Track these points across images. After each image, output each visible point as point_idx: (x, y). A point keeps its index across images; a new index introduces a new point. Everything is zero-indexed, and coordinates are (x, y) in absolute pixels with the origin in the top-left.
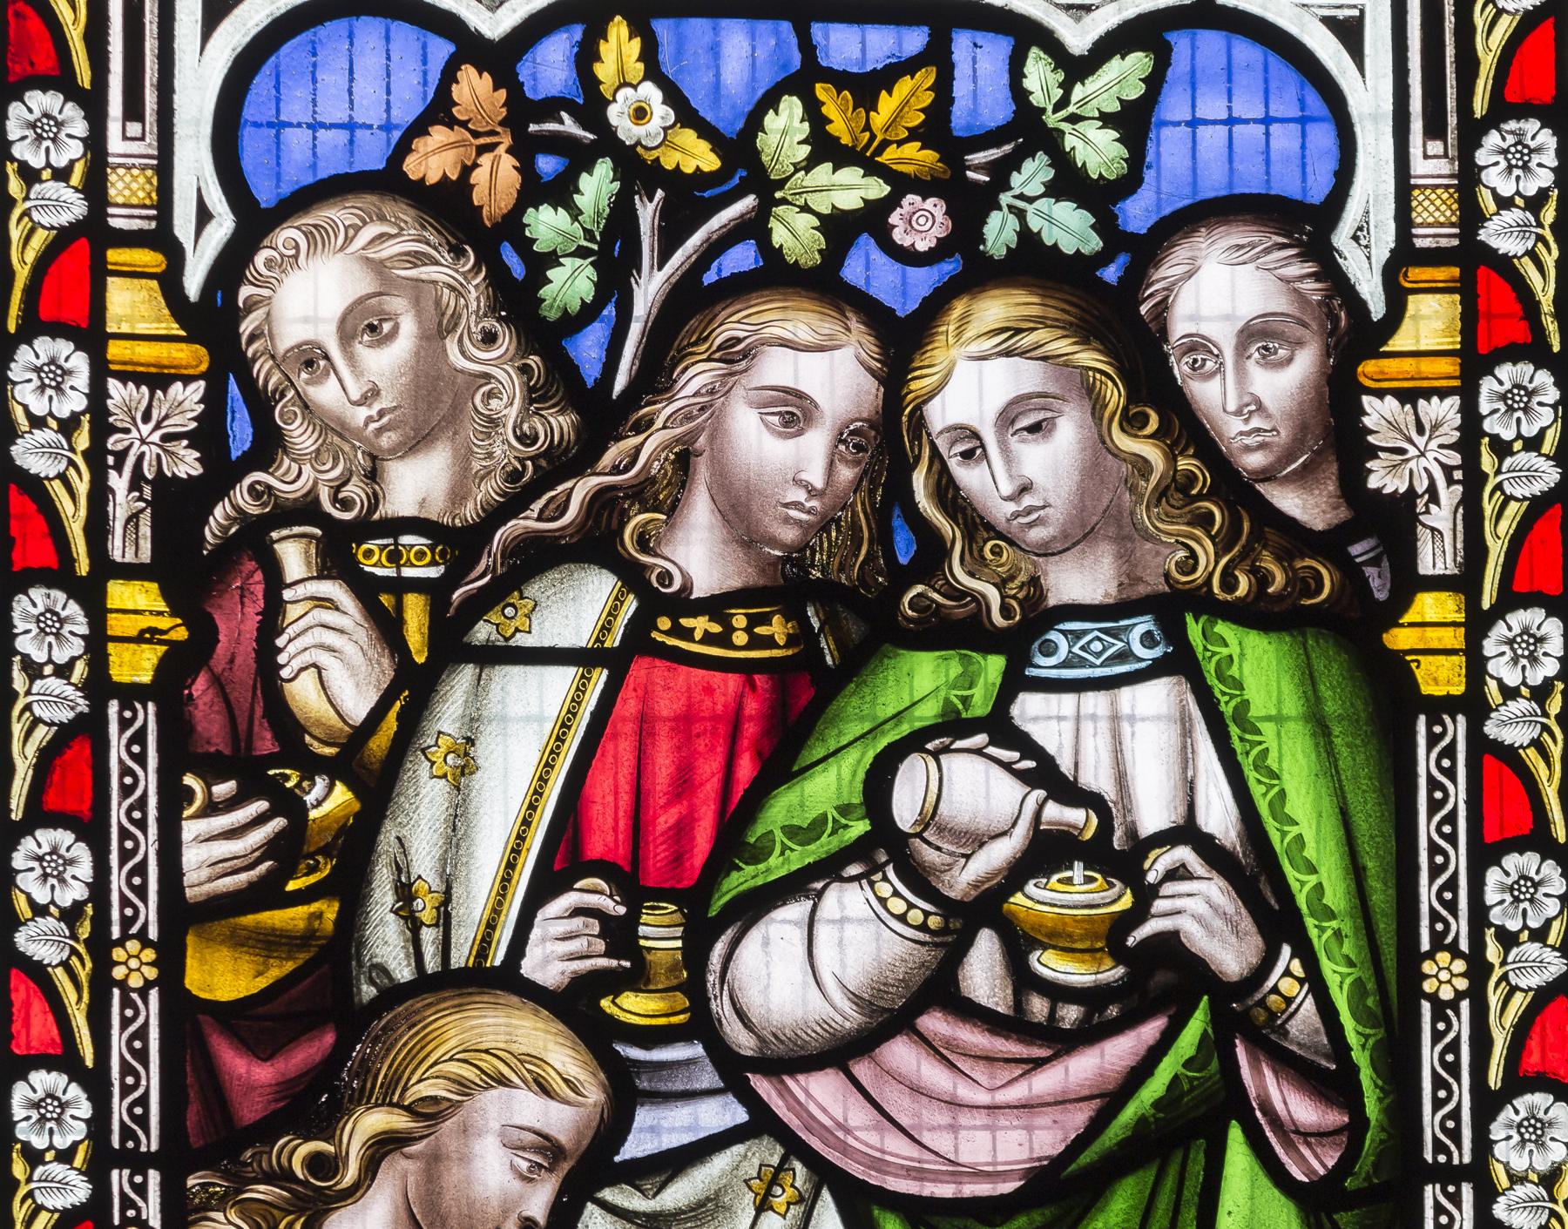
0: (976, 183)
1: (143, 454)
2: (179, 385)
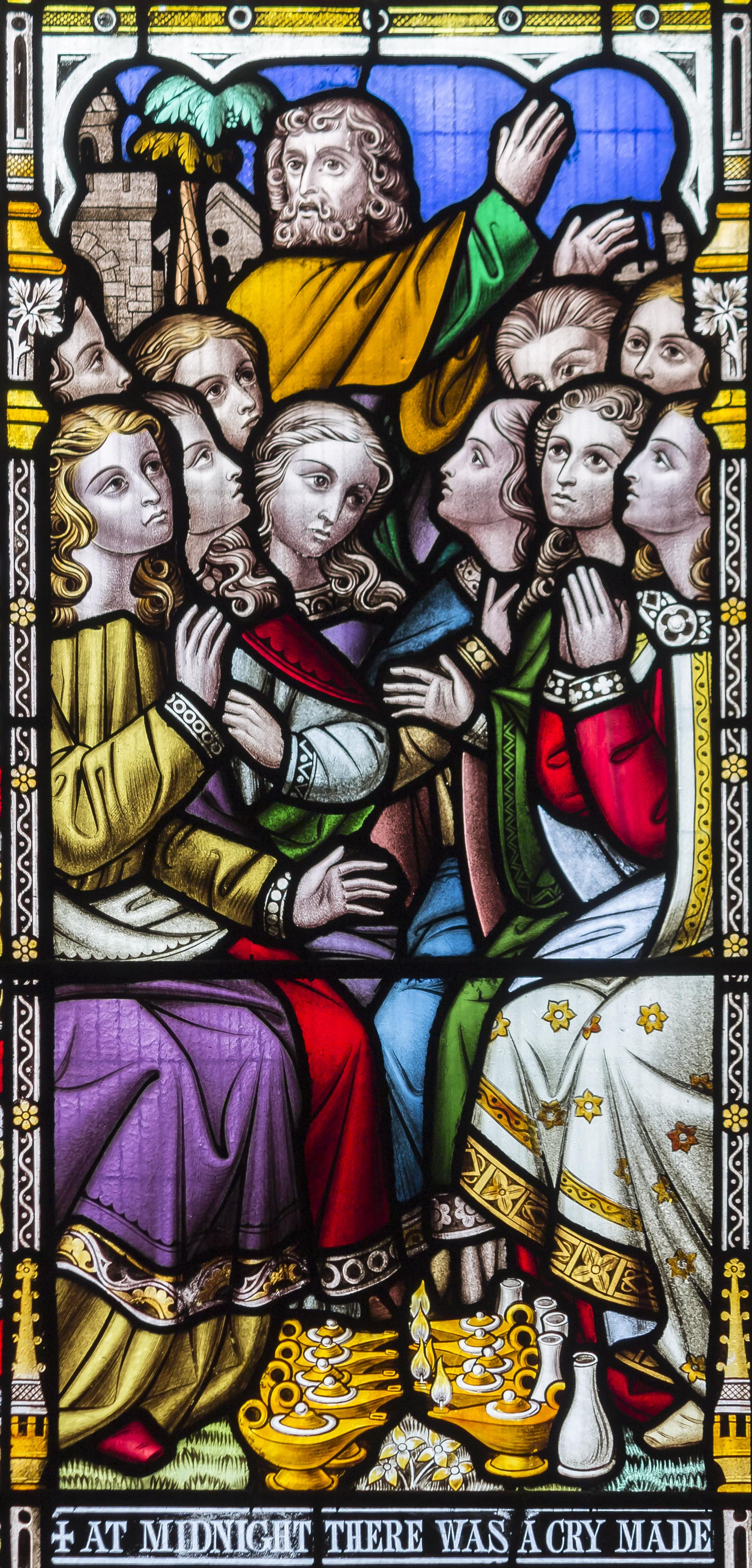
0: (315, 621)
1: (27, 322)
2: (48, 280)
